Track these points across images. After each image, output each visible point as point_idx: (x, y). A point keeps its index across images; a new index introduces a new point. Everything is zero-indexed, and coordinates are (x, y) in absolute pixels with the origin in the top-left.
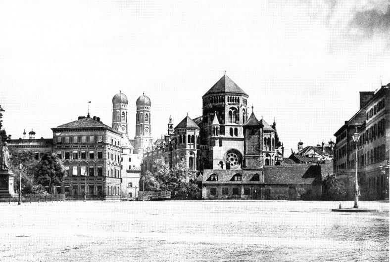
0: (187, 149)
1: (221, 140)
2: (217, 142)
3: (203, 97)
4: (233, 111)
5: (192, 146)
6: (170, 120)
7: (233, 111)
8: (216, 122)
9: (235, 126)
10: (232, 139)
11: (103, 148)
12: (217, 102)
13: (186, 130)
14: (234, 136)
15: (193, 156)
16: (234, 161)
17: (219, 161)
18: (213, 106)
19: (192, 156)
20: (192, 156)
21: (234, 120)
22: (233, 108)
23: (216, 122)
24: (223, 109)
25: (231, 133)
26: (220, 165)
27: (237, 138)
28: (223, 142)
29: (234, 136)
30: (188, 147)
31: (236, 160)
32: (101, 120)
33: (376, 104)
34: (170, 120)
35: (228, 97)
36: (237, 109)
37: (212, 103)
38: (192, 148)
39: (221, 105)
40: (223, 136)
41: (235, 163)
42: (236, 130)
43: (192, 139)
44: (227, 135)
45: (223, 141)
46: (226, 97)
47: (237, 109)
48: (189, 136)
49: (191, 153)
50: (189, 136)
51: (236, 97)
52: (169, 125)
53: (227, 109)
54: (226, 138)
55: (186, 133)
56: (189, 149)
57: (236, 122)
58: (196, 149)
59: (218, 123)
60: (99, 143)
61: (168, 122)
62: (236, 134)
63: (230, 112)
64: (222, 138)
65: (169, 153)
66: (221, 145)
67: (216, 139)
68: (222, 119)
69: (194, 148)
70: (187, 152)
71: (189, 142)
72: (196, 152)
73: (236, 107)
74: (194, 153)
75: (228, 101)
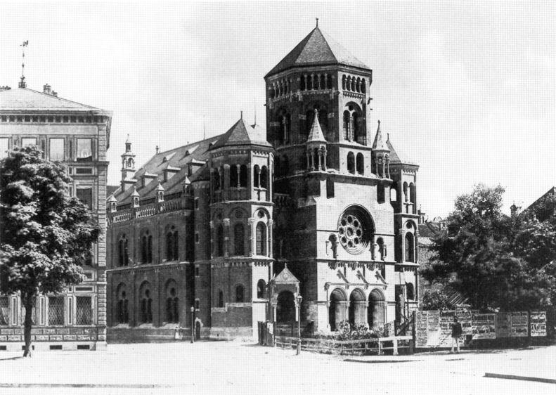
0: (252, 200)
1: (331, 180)
2: (323, 184)
3: (266, 78)
4: (351, 112)
5: (263, 195)
6: (128, 146)
7: (351, 112)
8: (318, 134)
9: (356, 148)
10: (354, 180)
11: (96, 177)
12: (316, 87)
13: (248, 152)
14: (357, 175)
15: (265, 220)
16: (355, 236)
17: (328, 234)
18: (305, 97)
19: (262, 220)
20: (262, 220)
21: (351, 135)
22: (351, 105)
23: (318, 134)
24: (335, 102)
25: (350, 167)
26: (330, 244)
27: (360, 179)
28: (338, 186)
29: (357, 175)
30: (254, 198)
31: (358, 233)
32: (52, 89)
33: (238, 172)
34: (128, 146)
35: (344, 76)
36: (361, 107)
37: (302, 89)
38: (263, 200)
39: (328, 95)
40: (336, 173)
41: (356, 240)
42: (360, 157)
43: (262, 175)
44: (343, 170)
45: (335, 184)
46: (340, 75)
47: (361, 107)
48: (256, 166)
49: (262, 213)
50: (256, 166)
51: (359, 78)
52: (124, 156)
53: (343, 107)
54: (341, 177)
55: (248, 160)
56: (256, 200)
57: (356, 140)
58: (271, 202)
59: (324, 140)
60: (79, 160)
61: (124, 152)
62: (361, 170)
63: (346, 113)
64: (334, 176)
65: (186, 213)
66: (330, 194)
67: (320, 176)
68: (329, 127)
69: (268, 198)
70: (254, 208)
71: (256, 185)
72: (270, 209)
73: (358, 101)
74: (267, 213)
75: (344, 88)
